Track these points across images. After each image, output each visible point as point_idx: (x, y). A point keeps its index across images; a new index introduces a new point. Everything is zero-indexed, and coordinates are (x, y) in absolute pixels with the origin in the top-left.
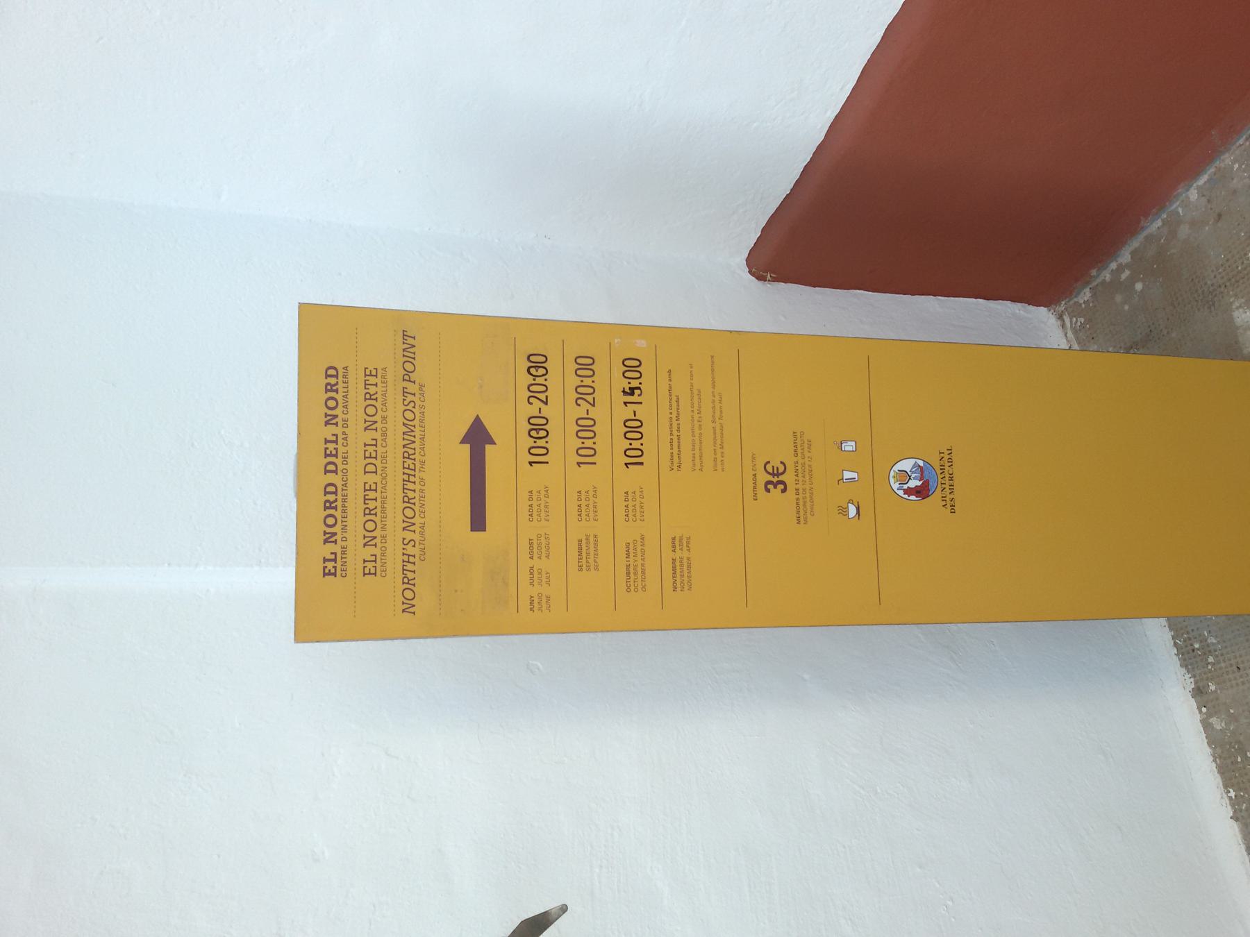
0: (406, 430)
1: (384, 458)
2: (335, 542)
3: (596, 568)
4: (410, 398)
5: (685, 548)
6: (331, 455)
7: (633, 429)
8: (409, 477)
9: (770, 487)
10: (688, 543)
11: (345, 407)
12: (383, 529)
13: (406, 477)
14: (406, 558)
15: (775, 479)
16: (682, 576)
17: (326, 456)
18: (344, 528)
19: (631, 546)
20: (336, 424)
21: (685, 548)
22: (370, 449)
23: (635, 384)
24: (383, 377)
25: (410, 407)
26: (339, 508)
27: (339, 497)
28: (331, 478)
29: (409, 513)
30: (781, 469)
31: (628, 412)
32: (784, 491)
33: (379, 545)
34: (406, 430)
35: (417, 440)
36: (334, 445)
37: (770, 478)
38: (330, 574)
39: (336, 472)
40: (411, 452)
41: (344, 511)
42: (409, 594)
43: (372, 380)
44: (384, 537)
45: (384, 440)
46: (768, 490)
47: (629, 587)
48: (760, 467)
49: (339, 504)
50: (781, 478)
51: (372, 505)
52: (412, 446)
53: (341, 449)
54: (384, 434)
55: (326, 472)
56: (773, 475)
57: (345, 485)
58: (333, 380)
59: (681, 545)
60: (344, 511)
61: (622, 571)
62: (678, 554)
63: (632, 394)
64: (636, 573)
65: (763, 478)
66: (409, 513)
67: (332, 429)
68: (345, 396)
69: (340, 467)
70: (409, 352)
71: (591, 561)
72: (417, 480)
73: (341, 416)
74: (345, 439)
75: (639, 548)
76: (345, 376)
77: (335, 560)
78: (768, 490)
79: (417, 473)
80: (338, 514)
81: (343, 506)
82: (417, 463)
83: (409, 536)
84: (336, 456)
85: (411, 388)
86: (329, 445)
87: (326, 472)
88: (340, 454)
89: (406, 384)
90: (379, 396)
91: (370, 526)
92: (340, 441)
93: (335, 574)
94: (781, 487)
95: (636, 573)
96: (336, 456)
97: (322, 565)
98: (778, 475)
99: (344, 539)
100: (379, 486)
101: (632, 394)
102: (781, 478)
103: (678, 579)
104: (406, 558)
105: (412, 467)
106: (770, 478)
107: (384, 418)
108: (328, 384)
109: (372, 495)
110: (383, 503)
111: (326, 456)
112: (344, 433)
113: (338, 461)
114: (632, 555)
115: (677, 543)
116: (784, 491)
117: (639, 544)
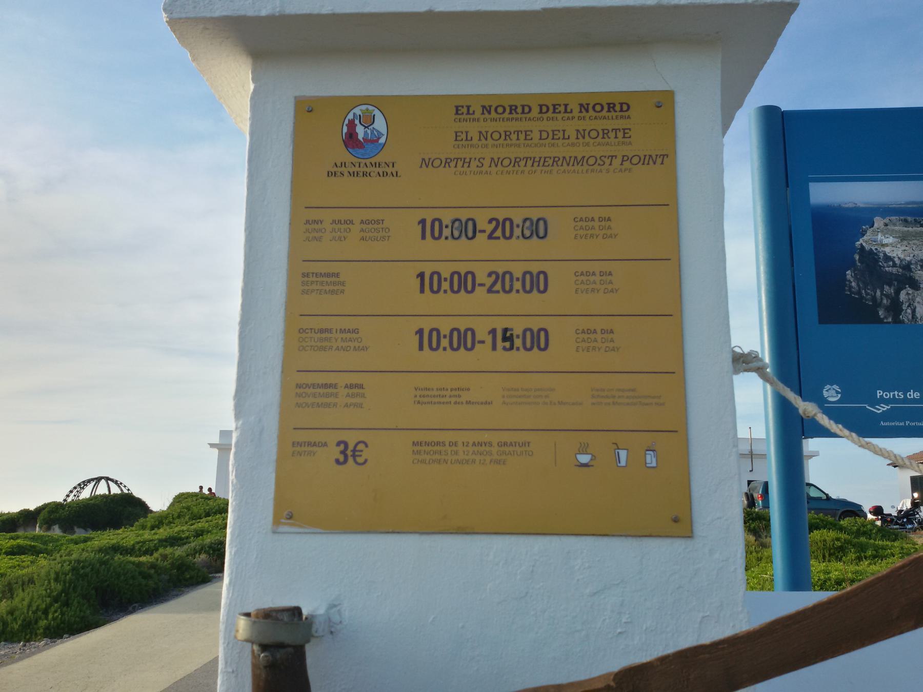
0: (579, 158)
1: (553, 145)
2: (483, 113)
3: (304, 292)
4: (608, 161)
5: (350, 400)
6: (555, 109)
7: (463, 340)
8: (541, 162)
9: (342, 447)
10: (355, 405)
11: (596, 118)
12: (493, 145)
13: (537, 159)
14: (467, 160)
15: (349, 453)
16: (314, 395)
17: (554, 106)
18: (495, 120)
19: (354, 336)
20: (581, 112)
21: (350, 400)
22: (561, 135)
23: (518, 342)
24: (623, 143)
25: (599, 161)
26: (511, 116)
27: (519, 116)
28: (536, 110)
29: (506, 162)
30: (360, 460)
31: (482, 334)
32: (337, 461)
33: (480, 143)
34: (579, 158)
35: (570, 167)
36: (465, 138)
37: (351, 447)
38: (457, 110)
39: (541, 112)
40: (560, 163)
41: (508, 119)
42: (437, 163)
43: (620, 134)
44: (486, 146)
45: (568, 145)
46: (338, 444)
47: (304, 331)
48: (362, 436)
49: (514, 116)
50: (351, 460)
51: (514, 137)
52: (565, 163)
53: (559, 116)
54: (573, 145)
55: (541, 106)
56: (354, 451)
57: (530, 119)
58: (625, 107)
59: (353, 396)
60: (508, 119)
61: (325, 323)
62: (343, 392)
63: (505, 339)
64: (321, 340)
65: (352, 439)
66: (506, 162)
67: (576, 109)
68: (605, 118)
69: (545, 116)
70: (648, 159)
71: (314, 287)
72: (534, 169)
73: (588, 115)
74: (568, 118)
75: (352, 344)
76: (622, 117)
77: (468, 113)
78: (338, 444)
79: (541, 168)
80: (506, 115)
81: (512, 119)
82: (550, 168)
83: (487, 163)
84: (554, 112)
85: (617, 162)
86: (464, 134)
87: (541, 106)
88: (555, 115)
89: (619, 159)
90: (607, 140)
91: (496, 136)
92: (566, 115)
93: (457, 113)
94: (342, 459)
95: (321, 340)
96: (554, 112)
97: (465, 104)
98: (354, 456)
99: (485, 120)
100: (530, 142)
101: (505, 339)
102: (351, 460)
103: (312, 390)
104: (467, 160)
105: (546, 164)
106: (351, 447)
107: (588, 144)
108: (614, 105)
109: (522, 136)
110: (516, 145)
111: (554, 106)
112: (573, 118)
113: (550, 114)
114: (344, 336)
115: (356, 391)
116: (337, 461)
117: (357, 344)
